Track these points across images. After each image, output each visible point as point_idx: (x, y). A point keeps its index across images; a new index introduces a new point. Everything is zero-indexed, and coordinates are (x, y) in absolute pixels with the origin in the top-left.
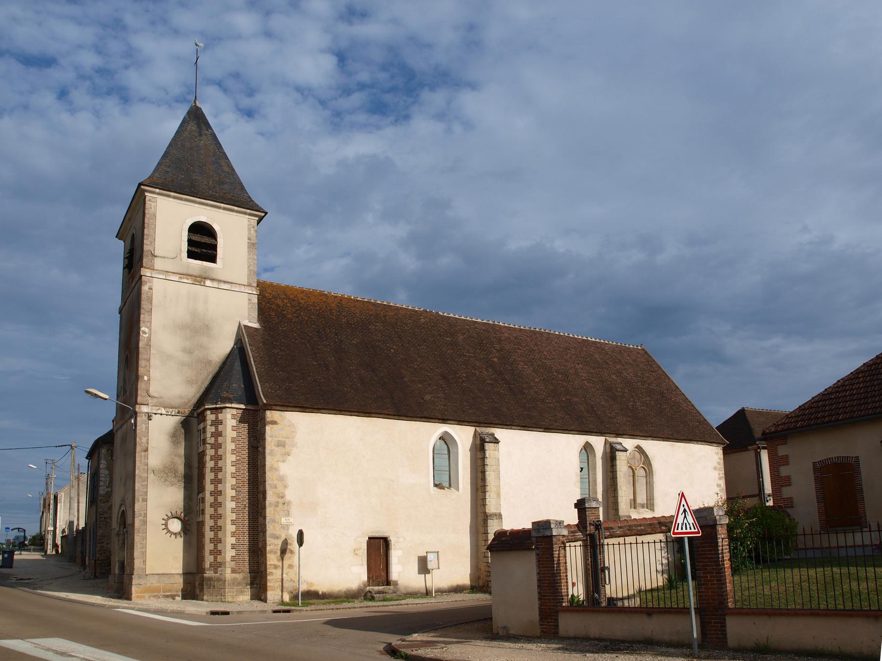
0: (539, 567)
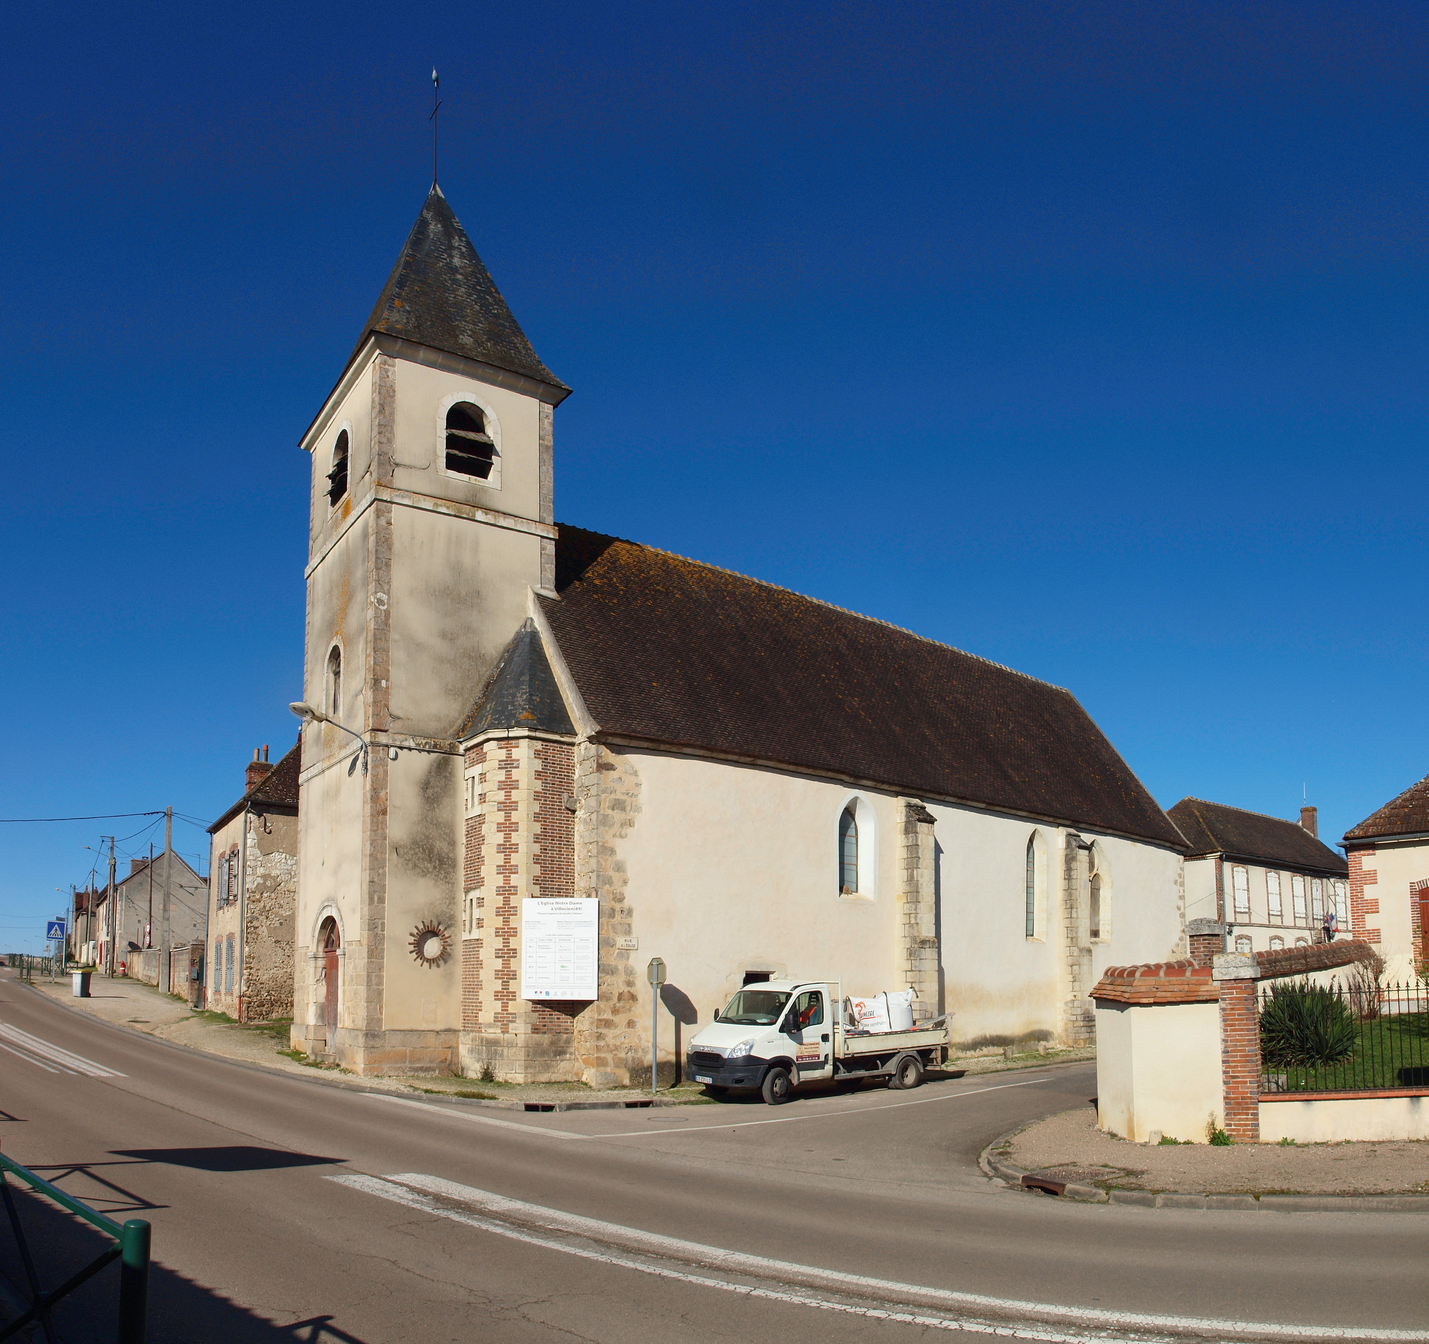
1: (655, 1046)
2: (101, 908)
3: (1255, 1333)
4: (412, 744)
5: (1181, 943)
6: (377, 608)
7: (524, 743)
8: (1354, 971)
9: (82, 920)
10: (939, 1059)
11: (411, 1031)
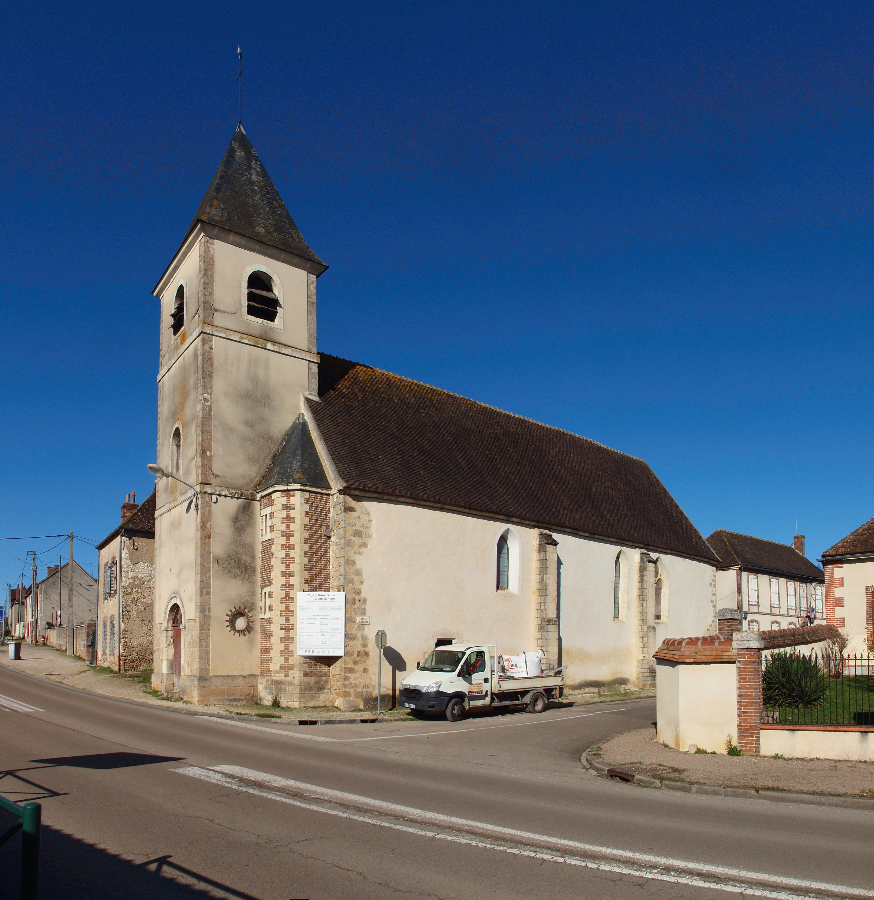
0: (740, 682)
1: (380, 685)
2: (28, 599)
3: (753, 879)
4: (227, 493)
5: (713, 624)
6: (203, 404)
7: (298, 493)
8: (826, 646)
9: (15, 607)
10: (558, 695)
11: (228, 676)
